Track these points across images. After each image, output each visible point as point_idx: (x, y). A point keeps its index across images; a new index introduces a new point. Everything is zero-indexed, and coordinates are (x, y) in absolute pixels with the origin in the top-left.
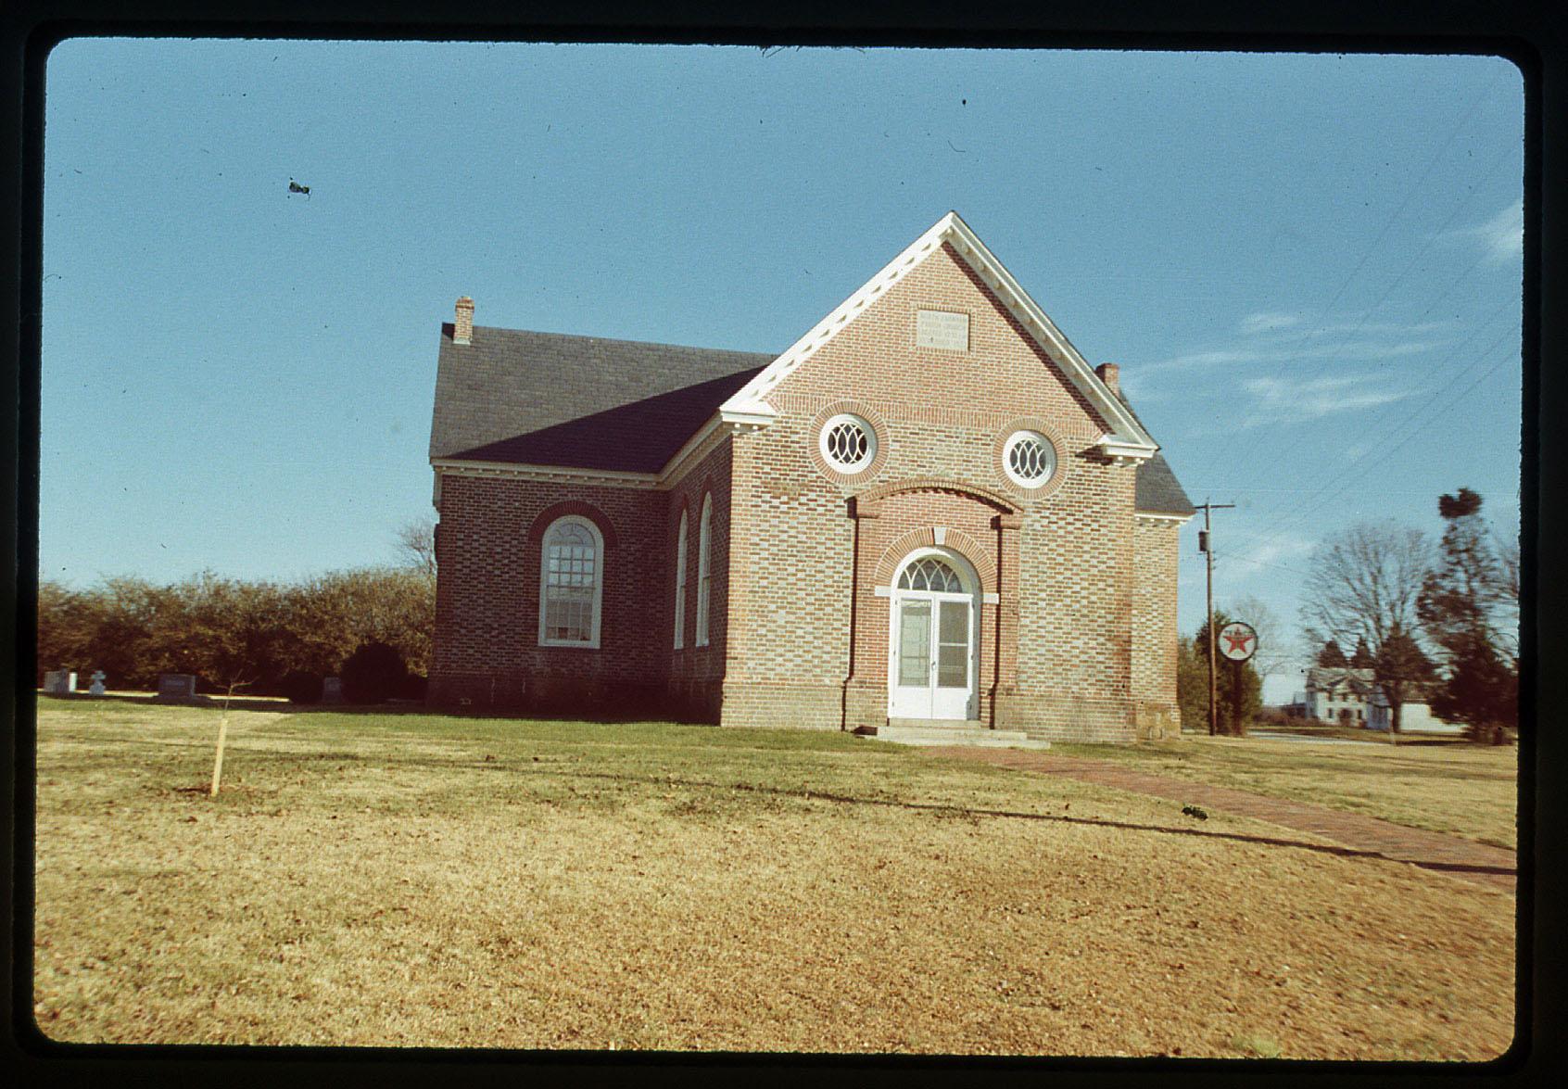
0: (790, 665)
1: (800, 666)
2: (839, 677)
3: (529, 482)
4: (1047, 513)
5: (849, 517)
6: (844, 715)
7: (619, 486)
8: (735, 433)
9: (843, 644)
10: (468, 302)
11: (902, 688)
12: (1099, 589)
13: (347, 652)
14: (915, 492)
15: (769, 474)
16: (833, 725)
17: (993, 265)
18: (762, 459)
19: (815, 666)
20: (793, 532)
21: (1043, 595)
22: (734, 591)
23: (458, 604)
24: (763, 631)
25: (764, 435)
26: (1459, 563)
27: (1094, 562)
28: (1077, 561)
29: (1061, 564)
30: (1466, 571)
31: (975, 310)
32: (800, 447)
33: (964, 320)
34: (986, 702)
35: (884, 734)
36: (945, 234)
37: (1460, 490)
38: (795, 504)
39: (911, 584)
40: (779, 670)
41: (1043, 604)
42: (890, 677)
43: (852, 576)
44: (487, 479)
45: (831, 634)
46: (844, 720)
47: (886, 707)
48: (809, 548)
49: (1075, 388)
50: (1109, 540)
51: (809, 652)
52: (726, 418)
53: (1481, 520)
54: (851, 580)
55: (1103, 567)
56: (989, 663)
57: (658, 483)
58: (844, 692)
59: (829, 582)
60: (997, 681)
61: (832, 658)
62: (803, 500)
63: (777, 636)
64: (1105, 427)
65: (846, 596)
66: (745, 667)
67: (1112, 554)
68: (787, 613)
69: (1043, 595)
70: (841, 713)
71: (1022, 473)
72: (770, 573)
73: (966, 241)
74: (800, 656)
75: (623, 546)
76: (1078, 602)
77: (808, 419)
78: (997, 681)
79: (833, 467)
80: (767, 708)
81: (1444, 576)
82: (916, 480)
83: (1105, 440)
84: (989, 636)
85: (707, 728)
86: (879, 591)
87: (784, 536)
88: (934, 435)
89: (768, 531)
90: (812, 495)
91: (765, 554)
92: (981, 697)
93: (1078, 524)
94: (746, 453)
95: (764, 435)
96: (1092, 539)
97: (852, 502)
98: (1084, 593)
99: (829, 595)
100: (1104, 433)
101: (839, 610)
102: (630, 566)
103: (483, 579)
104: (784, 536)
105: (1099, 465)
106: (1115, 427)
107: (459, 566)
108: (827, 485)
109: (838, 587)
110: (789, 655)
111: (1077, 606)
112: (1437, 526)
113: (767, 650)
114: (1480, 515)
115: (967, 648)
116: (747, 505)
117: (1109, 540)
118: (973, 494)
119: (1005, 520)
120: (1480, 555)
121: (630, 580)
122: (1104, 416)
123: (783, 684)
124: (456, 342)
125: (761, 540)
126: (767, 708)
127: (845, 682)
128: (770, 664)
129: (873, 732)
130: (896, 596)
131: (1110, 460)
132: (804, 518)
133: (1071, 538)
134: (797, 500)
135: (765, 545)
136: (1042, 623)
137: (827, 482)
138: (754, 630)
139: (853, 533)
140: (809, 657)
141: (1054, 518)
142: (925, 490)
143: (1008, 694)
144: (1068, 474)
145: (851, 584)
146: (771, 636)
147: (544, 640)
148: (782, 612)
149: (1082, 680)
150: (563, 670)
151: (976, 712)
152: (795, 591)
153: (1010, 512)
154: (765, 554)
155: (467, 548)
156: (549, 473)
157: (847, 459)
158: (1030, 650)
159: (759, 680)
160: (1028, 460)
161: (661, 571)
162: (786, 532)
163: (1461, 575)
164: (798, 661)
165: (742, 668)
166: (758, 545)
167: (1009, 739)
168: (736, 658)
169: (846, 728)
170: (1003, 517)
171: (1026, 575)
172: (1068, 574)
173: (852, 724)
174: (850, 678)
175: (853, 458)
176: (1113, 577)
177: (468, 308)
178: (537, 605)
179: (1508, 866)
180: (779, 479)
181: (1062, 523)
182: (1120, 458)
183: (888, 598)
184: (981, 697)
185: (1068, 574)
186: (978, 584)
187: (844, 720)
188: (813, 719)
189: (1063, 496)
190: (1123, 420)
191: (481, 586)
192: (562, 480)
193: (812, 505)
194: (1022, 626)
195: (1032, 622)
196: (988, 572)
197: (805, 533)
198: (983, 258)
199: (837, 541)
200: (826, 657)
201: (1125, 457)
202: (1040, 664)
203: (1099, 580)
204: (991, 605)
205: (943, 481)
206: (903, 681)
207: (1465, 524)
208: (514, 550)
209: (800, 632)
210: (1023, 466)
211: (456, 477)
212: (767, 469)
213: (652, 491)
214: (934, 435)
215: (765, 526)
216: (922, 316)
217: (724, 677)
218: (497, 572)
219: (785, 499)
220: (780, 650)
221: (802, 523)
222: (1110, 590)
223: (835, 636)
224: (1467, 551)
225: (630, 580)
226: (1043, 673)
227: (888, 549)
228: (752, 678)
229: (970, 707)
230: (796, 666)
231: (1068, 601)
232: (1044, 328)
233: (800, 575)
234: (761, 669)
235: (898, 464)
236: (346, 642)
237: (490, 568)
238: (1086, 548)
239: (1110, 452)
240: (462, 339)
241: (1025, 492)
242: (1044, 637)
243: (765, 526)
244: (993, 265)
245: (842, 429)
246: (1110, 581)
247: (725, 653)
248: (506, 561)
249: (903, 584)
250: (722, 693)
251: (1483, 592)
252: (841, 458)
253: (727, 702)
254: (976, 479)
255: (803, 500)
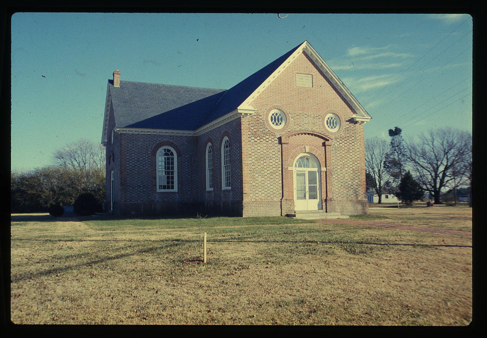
0: (263, 195)
1: (266, 195)
2: (279, 198)
3: (150, 135)
4: (339, 140)
5: (279, 144)
6: (281, 211)
7: (181, 135)
8: (242, 117)
9: (279, 187)
10: (118, 72)
11: (298, 200)
12: (355, 165)
13: (44, 196)
14: (302, 134)
15: (253, 130)
16: (278, 214)
17: (320, 59)
18: (251, 125)
19: (271, 195)
20: (262, 149)
21: (339, 167)
22: (244, 170)
23: (128, 179)
24: (254, 184)
25: (251, 117)
26: (395, 150)
27: (353, 156)
28: (348, 156)
29: (344, 157)
30: (398, 153)
31: (314, 74)
32: (263, 121)
33: (311, 77)
34: (324, 204)
35: (298, 217)
36: (304, 49)
37: (395, 128)
38: (262, 140)
39: (297, 166)
40: (260, 197)
41: (339, 170)
42: (294, 197)
43: (281, 164)
44: (136, 134)
45: (275, 184)
46: (281, 212)
47: (294, 207)
48: (267, 155)
49: (345, 99)
50: (357, 148)
51: (269, 190)
52: (239, 111)
53: (402, 136)
54: (281, 165)
55: (356, 157)
56: (324, 190)
57: (194, 134)
58: (281, 203)
59: (274, 166)
60: (327, 196)
61: (276, 192)
62: (264, 138)
63: (259, 185)
64: (354, 112)
65: (280, 171)
66: (249, 196)
67: (358, 153)
68: (261, 177)
69: (339, 167)
70: (280, 210)
71: (330, 127)
72: (255, 164)
73: (311, 51)
74: (266, 192)
75: (184, 156)
76: (349, 169)
77: (265, 111)
78: (327, 196)
79: (273, 127)
80: (257, 210)
81: (391, 154)
82: (299, 131)
83: (354, 116)
84: (324, 182)
85: (239, 218)
86: (290, 168)
87: (259, 151)
88: (304, 116)
89: (254, 149)
90: (267, 137)
91: (253, 157)
92: (322, 202)
93: (348, 143)
94: (245, 123)
95: (251, 117)
96: (353, 148)
97: (280, 139)
98: (351, 166)
99: (274, 171)
100: (354, 114)
101: (278, 175)
102: (186, 163)
103: (137, 169)
104: (259, 151)
105: (353, 124)
106: (357, 112)
107: (128, 165)
108: (272, 133)
109: (277, 167)
110: (263, 192)
111: (349, 171)
112: (389, 139)
113: (256, 190)
114: (401, 135)
115: (317, 186)
116: (247, 141)
117: (357, 148)
118: (317, 135)
119: (327, 143)
120: (402, 147)
121: (186, 168)
122: (354, 108)
123: (262, 201)
124: (115, 86)
125: (252, 153)
126: (257, 210)
127: (281, 200)
128: (257, 195)
129: (295, 216)
130: (294, 169)
131: (356, 122)
132: (265, 145)
133: (346, 148)
134: (263, 138)
135: (253, 154)
136: (339, 176)
137: (272, 132)
138: (251, 184)
139: (280, 149)
140: (269, 192)
141: (341, 142)
142: (302, 134)
143: (331, 201)
144: (344, 127)
145: (281, 166)
146: (257, 185)
147: (158, 190)
148: (260, 177)
149: (352, 195)
150: (166, 200)
151: (321, 207)
152: (263, 170)
153: (328, 140)
154: (253, 157)
155: (130, 159)
156: (158, 132)
157: (277, 124)
158: (336, 186)
159: (254, 200)
160: (331, 123)
161: (196, 164)
162: (260, 149)
163: (396, 154)
164: (266, 193)
165: (248, 197)
166: (251, 154)
167: (337, 215)
168: (246, 193)
169: (282, 215)
170: (326, 142)
171: (334, 161)
172: (346, 160)
173: (284, 213)
174: (282, 198)
175: (279, 124)
176: (359, 160)
177: (118, 74)
178: (156, 178)
179: (470, 245)
180: (256, 132)
181: (343, 143)
182: (360, 122)
183: (292, 171)
184: (322, 202)
185: (346, 160)
186: (319, 165)
187: (281, 212)
188: (272, 213)
189: (343, 135)
190: (360, 109)
191: (136, 172)
192: (162, 134)
193: (267, 140)
194: (333, 178)
195: (336, 176)
196: (322, 161)
197: (266, 150)
198: (316, 56)
199: (276, 152)
200: (274, 191)
201: (361, 121)
202: (339, 190)
203: (355, 162)
204: (324, 171)
205: (307, 131)
206: (298, 198)
207: (397, 138)
208: (147, 159)
209: (266, 184)
210: (275, 122)
211: (125, 134)
212: (252, 128)
213: (192, 137)
214: (304, 116)
215: (253, 148)
216: (298, 76)
217: (243, 200)
218: (141, 167)
219: (258, 138)
220: (260, 190)
221: (264, 146)
222: (358, 165)
223: (277, 184)
224: (397, 146)
225: (186, 168)
226: (340, 193)
227: (291, 154)
228: (251, 200)
229: (319, 205)
230: (265, 195)
231: (346, 169)
232: (335, 79)
233: (265, 164)
234: (254, 197)
235: (293, 127)
236: (44, 192)
237: (138, 165)
238: (351, 151)
239: (357, 120)
240: (117, 85)
241: (332, 133)
242: (340, 181)
243: (253, 148)
244: (320, 59)
245: (275, 114)
246: (358, 162)
247: (243, 192)
248: (144, 163)
249: (296, 166)
250: (243, 206)
251: (403, 159)
252: (275, 124)
253: (244, 209)
254: (317, 130)
255: (264, 138)
